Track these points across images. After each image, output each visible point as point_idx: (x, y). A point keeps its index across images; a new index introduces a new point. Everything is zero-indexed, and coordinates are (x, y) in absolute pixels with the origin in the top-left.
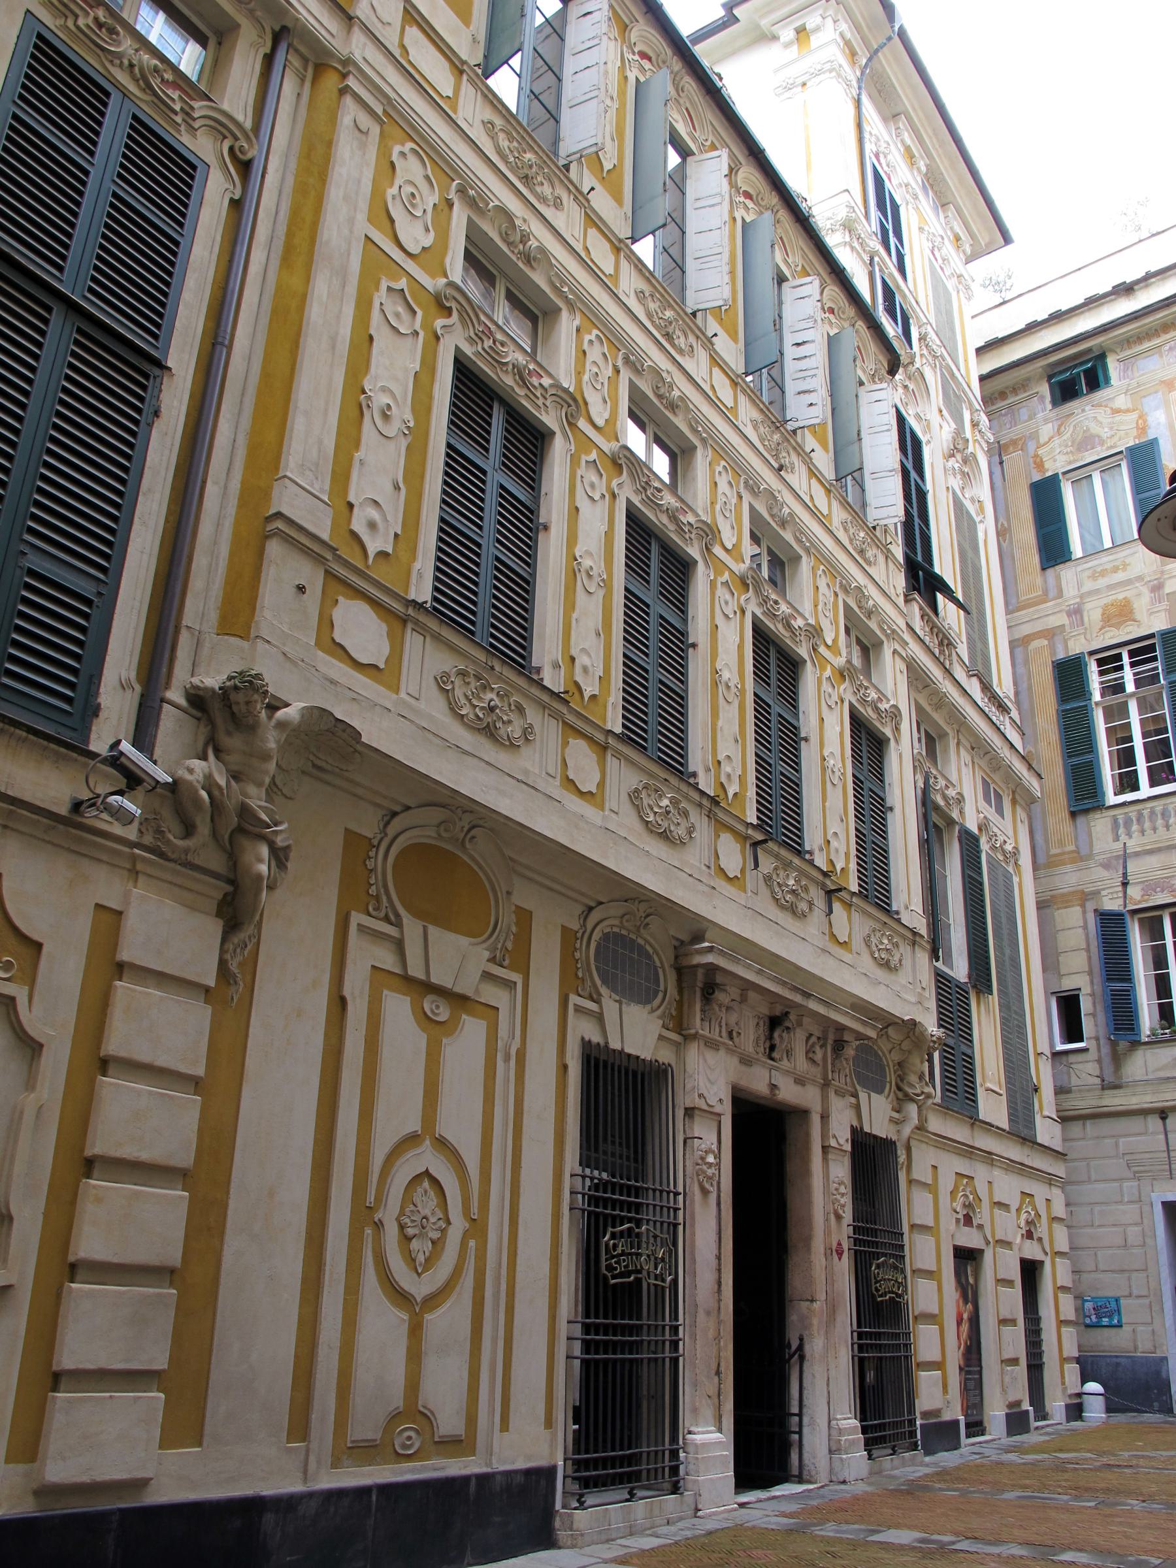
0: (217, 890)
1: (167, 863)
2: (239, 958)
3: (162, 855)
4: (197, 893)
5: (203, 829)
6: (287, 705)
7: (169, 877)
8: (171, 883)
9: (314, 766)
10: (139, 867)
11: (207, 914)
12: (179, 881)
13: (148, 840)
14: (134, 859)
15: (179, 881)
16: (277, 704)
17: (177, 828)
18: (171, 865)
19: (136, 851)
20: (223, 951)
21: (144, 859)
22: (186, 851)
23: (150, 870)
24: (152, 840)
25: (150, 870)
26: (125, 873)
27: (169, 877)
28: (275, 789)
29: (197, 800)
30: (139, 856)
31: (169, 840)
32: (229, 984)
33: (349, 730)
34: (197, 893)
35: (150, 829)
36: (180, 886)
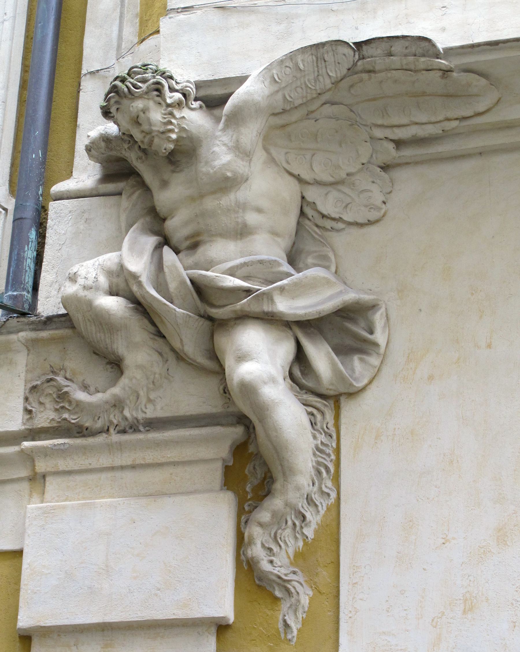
0: (217, 446)
1: (90, 441)
2: (292, 545)
3: (81, 431)
4: (175, 464)
5: (139, 355)
6: (241, 80)
7: (105, 461)
8: (112, 469)
9: (399, 144)
10: (41, 466)
11: (211, 491)
12: (126, 459)
13: (45, 417)
14: (29, 457)
15: (126, 459)
16: (219, 91)
17: (97, 374)
18: (100, 439)
19: (26, 444)
20: (241, 541)
21: (45, 452)
22: (117, 404)
23: (62, 464)
24: (52, 415)
25: (62, 464)
26: (25, 485)
27: (105, 461)
28: (328, 224)
29: (102, 320)
30: (32, 449)
31: (79, 404)
32: (276, 599)
33: (397, 47)
34: (175, 464)
35: (47, 401)
36: (133, 467)
